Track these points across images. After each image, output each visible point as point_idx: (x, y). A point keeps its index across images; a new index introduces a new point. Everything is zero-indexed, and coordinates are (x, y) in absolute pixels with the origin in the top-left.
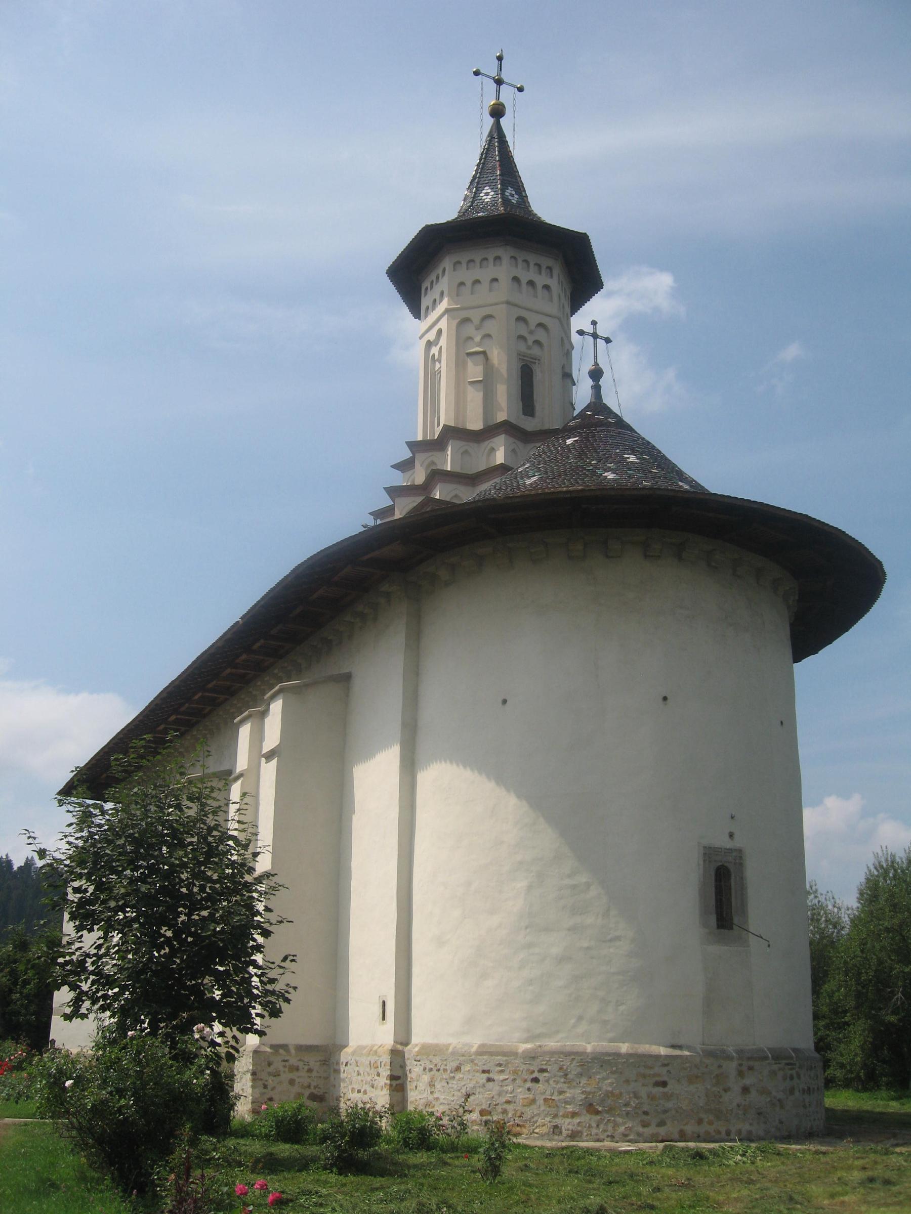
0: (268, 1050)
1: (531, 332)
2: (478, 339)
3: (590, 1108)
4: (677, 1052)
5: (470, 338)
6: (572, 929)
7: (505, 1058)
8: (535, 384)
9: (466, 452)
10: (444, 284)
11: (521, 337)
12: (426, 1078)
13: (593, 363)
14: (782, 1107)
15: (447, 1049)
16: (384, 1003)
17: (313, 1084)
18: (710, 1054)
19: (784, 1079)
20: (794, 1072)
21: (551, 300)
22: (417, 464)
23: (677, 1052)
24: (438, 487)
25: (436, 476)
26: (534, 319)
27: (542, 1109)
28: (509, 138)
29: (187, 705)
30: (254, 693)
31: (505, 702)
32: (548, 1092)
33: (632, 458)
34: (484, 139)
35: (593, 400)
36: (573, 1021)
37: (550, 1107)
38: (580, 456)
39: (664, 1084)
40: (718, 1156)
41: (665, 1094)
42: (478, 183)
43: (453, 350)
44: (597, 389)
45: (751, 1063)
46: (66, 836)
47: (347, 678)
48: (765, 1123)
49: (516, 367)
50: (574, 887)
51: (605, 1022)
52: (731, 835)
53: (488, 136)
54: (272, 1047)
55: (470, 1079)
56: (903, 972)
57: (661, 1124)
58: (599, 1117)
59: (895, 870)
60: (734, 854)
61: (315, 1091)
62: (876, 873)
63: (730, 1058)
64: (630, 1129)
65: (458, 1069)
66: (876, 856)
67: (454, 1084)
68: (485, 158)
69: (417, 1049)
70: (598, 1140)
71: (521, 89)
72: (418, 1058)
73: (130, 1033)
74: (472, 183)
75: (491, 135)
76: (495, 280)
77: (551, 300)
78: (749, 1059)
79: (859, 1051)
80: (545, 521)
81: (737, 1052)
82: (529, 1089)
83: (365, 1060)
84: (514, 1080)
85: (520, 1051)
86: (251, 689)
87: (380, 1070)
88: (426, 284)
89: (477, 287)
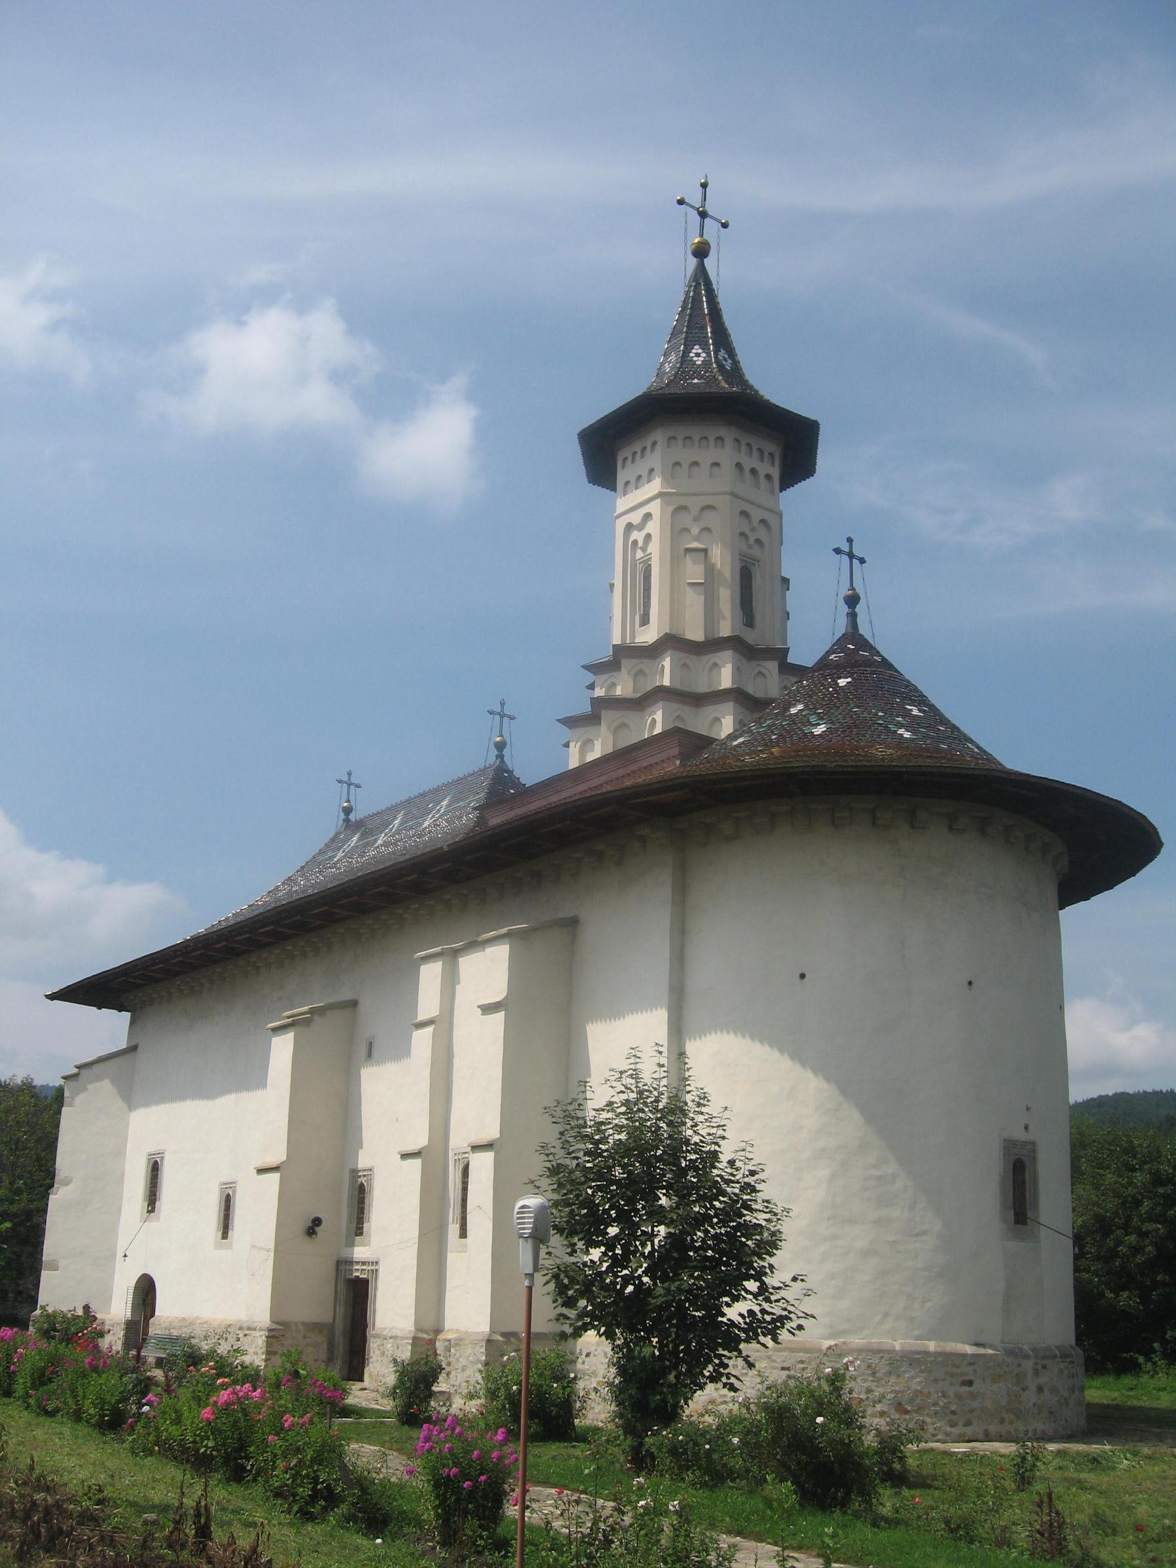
0: (500, 1338)
1: (753, 529)
2: (695, 530)
4: (981, 1351)
5: (687, 530)
6: (879, 1222)
11: (743, 534)
16: (225, 1235)
18: (1010, 1352)
23: (981, 1351)
31: (803, 976)
36: (878, 1318)
39: (970, 1383)
41: (971, 1394)
44: (853, 616)
47: (573, 923)
49: (738, 566)
50: (880, 1178)
51: (912, 1319)
52: (1026, 1127)
54: (503, 1334)
57: (968, 1423)
63: (1027, 1357)
71: (725, 226)
76: (716, 464)
78: (1044, 1357)
81: (1034, 1350)
85: (824, 1347)
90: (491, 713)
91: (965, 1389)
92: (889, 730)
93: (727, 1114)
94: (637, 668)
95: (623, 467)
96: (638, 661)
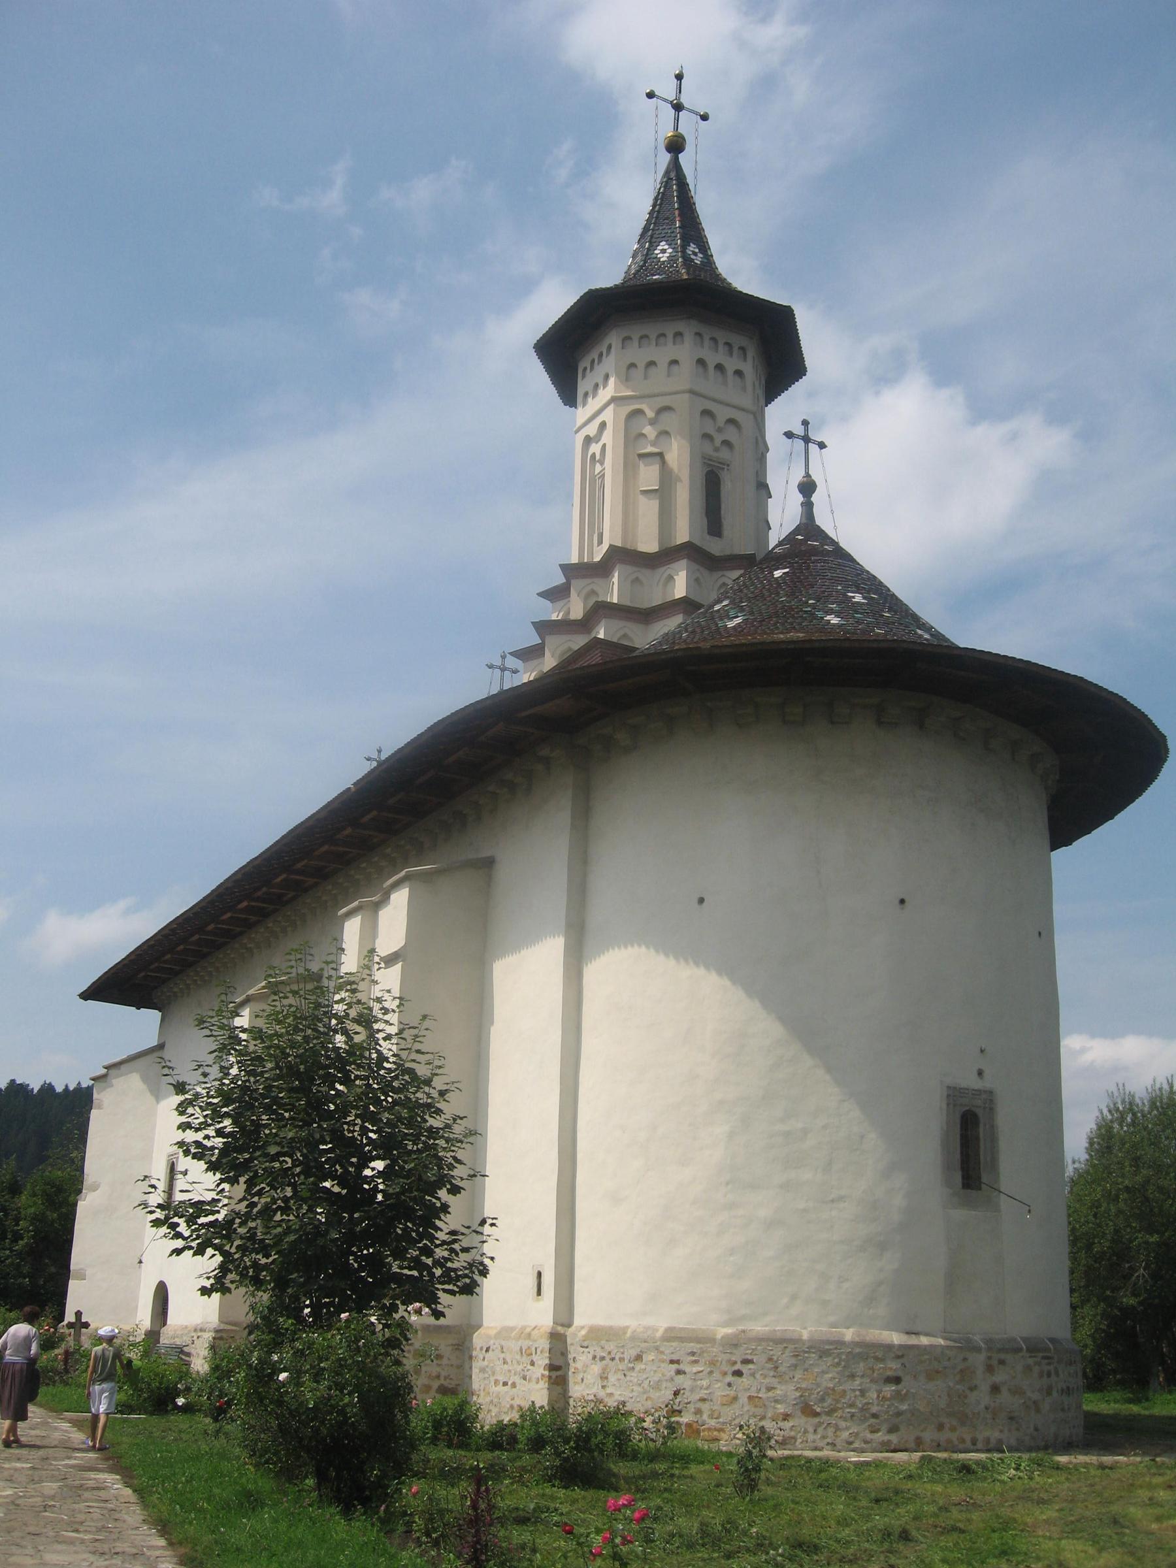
1: (720, 430)
3: (808, 1411)
7: (699, 1346)
8: (722, 494)
9: (637, 580)
10: (609, 363)
11: (707, 436)
12: (596, 1368)
13: (803, 473)
14: (1038, 1410)
15: (625, 1333)
16: (539, 1274)
17: (443, 1374)
19: (1041, 1376)
20: (1051, 1368)
21: (744, 389)
22: (573, 592)
23: (913, 1341)
24: (603, 623)
25: (600, 610)
26: (723, 414)
27: (746, 1409)
28: (690, 180)
29: (264, 889)
30: (357, 877)
31: (701, 901)
32: (754, 1389)
33: (858, 598)
34: (658, 181)
35: (804, 521)
36: (785, 1300)
37: (756, 1406)
38: (793, 593)
39: (897, 1380)
40: (988, 1470)
42: (652, 236)
43: (621, 451)
44: (808, 506)
45: (1002, 1356)
46: (200, 1066)
47: (489, 864)
48: (1018, 1429)
52: (980, 1073)
53: (664, 176)
55: (655, 1370)
56: (1147, 1243)
58: (817, 1420)
59: (1134, 1114)
60: (984, 1096)
61: (446, 1383)
62: (1110, 1117)
63: (978, 1350)
64: (857, 1434)
65: (639, 1358)
66: (1111, 1095)
67: (633, 1376)
68: (661, 205)
69: (583, 1332)
70: (816, 1449)
71: (704, 118)
72: (585, 1344)
73: (343, 1316)
74: (642, 235)
75: (667, 172)
76: (675, 362)
77: (744, 389)
79: (1089, 1342)
80: (753, 675)
82: (729, 1385)
83: (514, 1345)
84: (711, 1372)
85: (719, 1337)
86: (352, 872)
87: (535, 1358)
88: (584, 363)
89: (653, 370)
90: (491, 667)
91: (890, 1389)
92: (816, 617)
93: (426, 1024)
94: (588, 588)
95: (584, 376)
96: (588, 581)
